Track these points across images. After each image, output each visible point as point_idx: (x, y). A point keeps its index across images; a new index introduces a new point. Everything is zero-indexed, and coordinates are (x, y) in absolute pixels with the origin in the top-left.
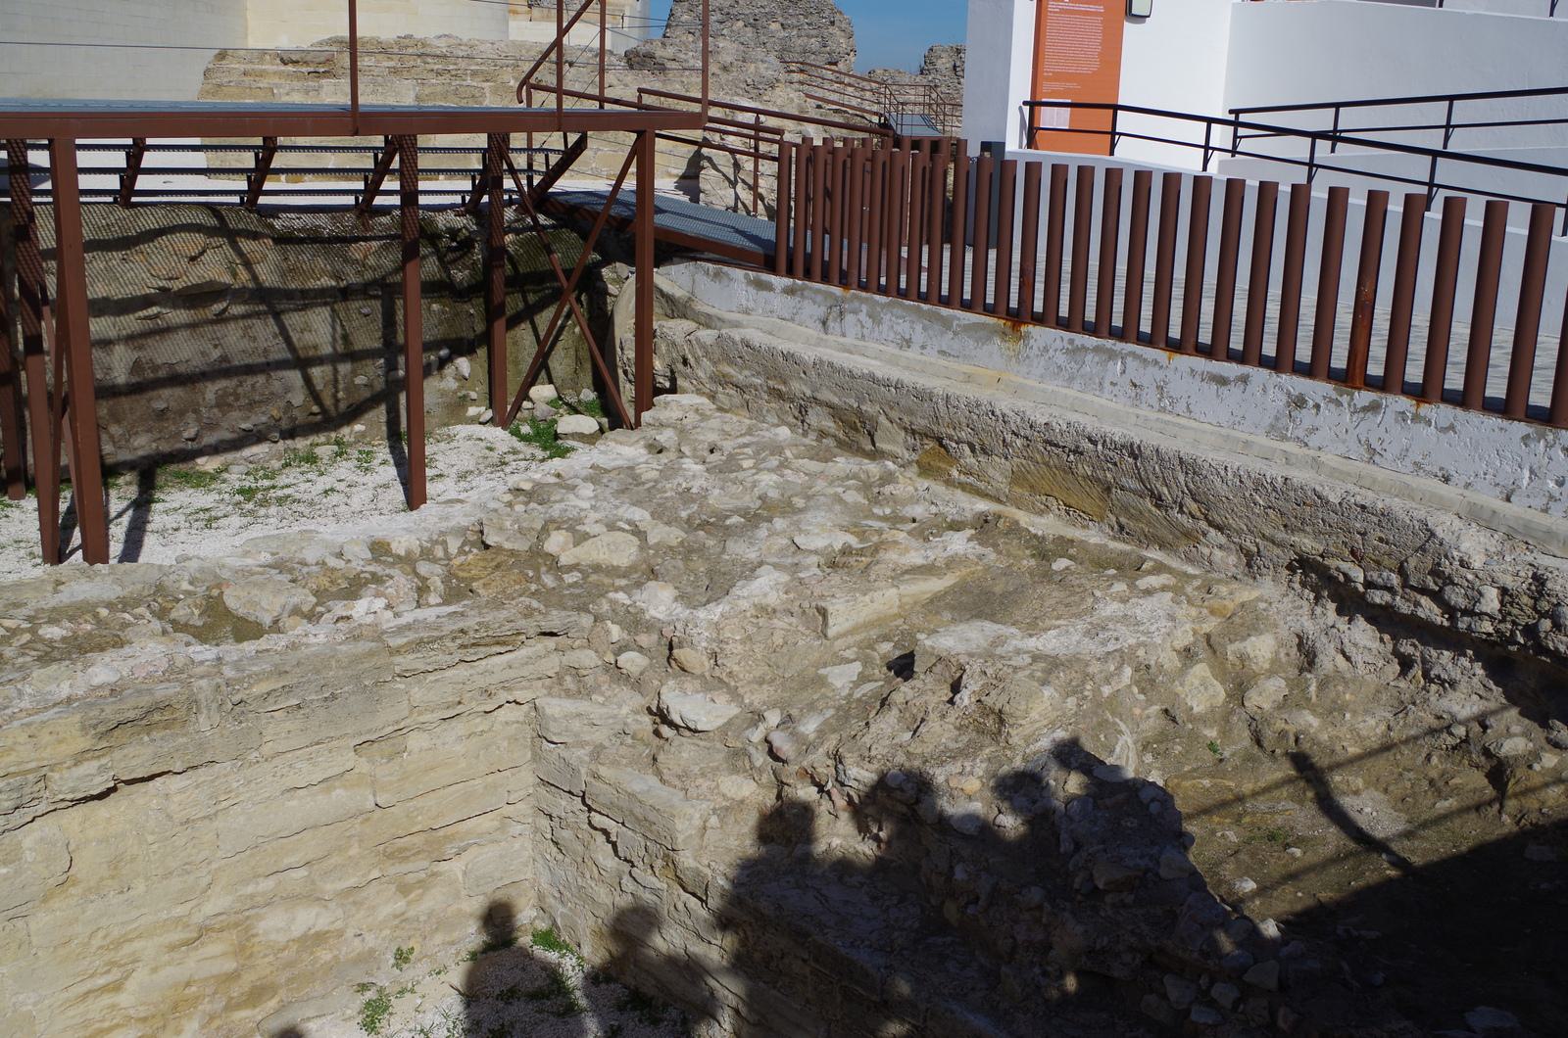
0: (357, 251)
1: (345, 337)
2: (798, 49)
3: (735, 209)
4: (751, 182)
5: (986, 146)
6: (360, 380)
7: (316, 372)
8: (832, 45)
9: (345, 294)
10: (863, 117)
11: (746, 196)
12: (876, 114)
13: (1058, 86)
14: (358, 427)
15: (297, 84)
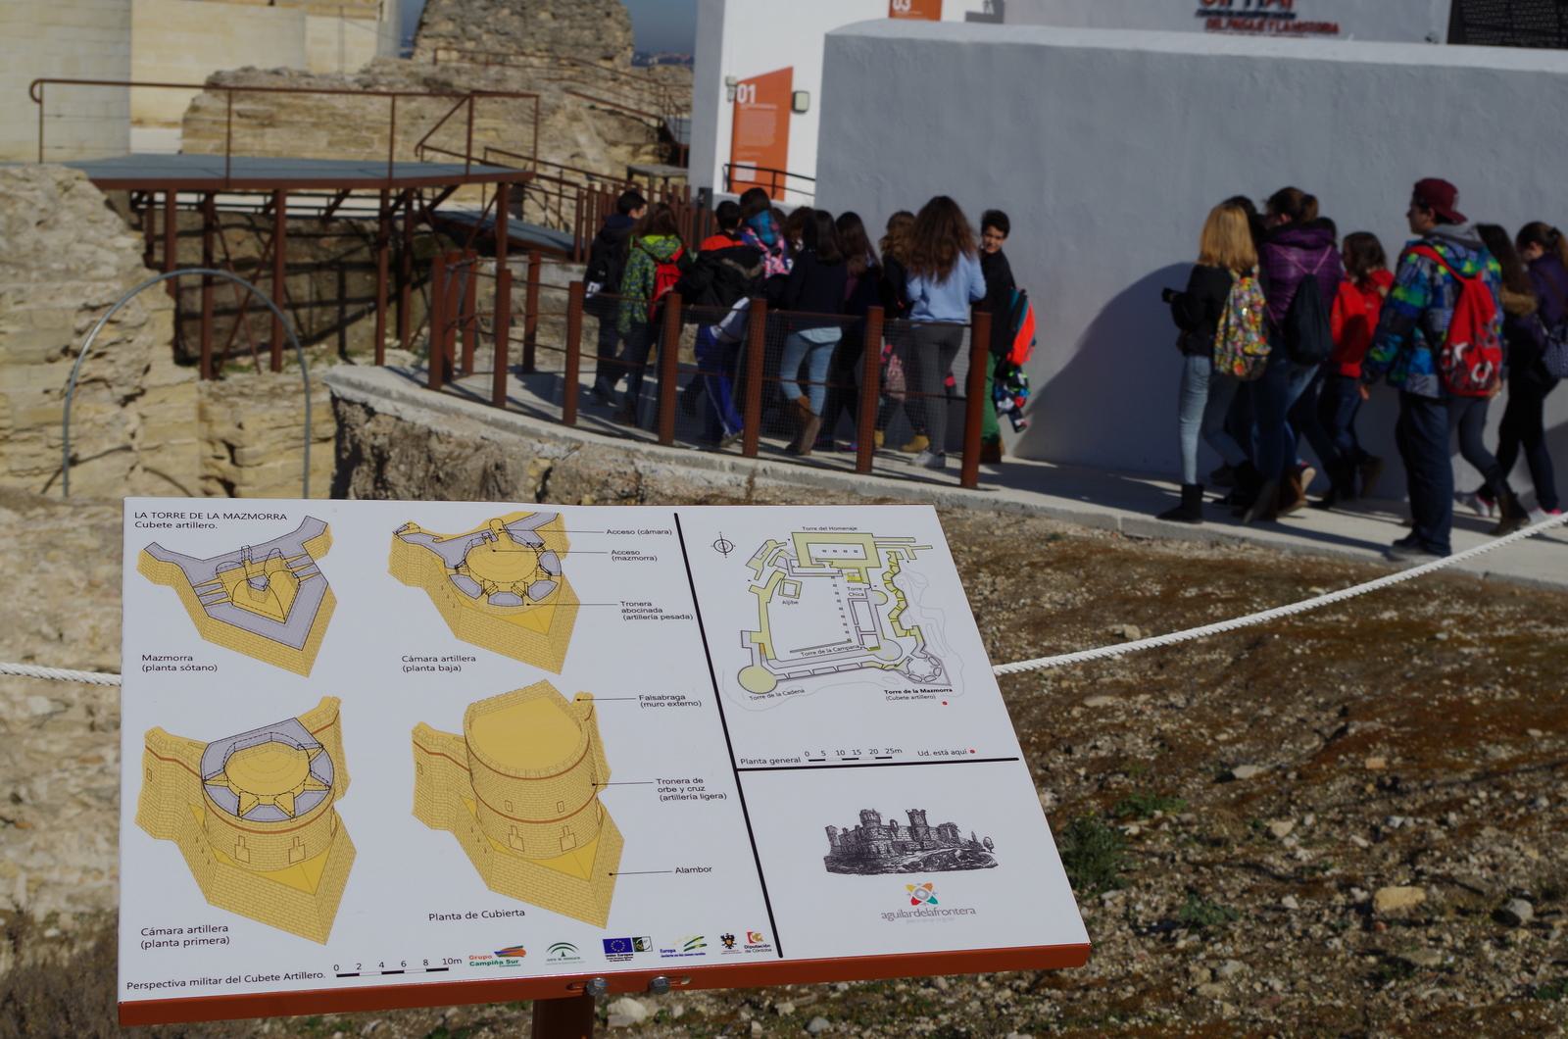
0: (325, 242)
1: (318, 293)
2: (570, 41)
3: (545, 225)
4: (556, 208)
5: (702, 191)
6: (326, 318)
7: (303, 312)
8: (607, 39)
9: (318, 267)
10: (640, 120)
11: (554, 218)
12: (653, 116)
13: (747, 154)
14: (323, 346)
15: (249, 131)
